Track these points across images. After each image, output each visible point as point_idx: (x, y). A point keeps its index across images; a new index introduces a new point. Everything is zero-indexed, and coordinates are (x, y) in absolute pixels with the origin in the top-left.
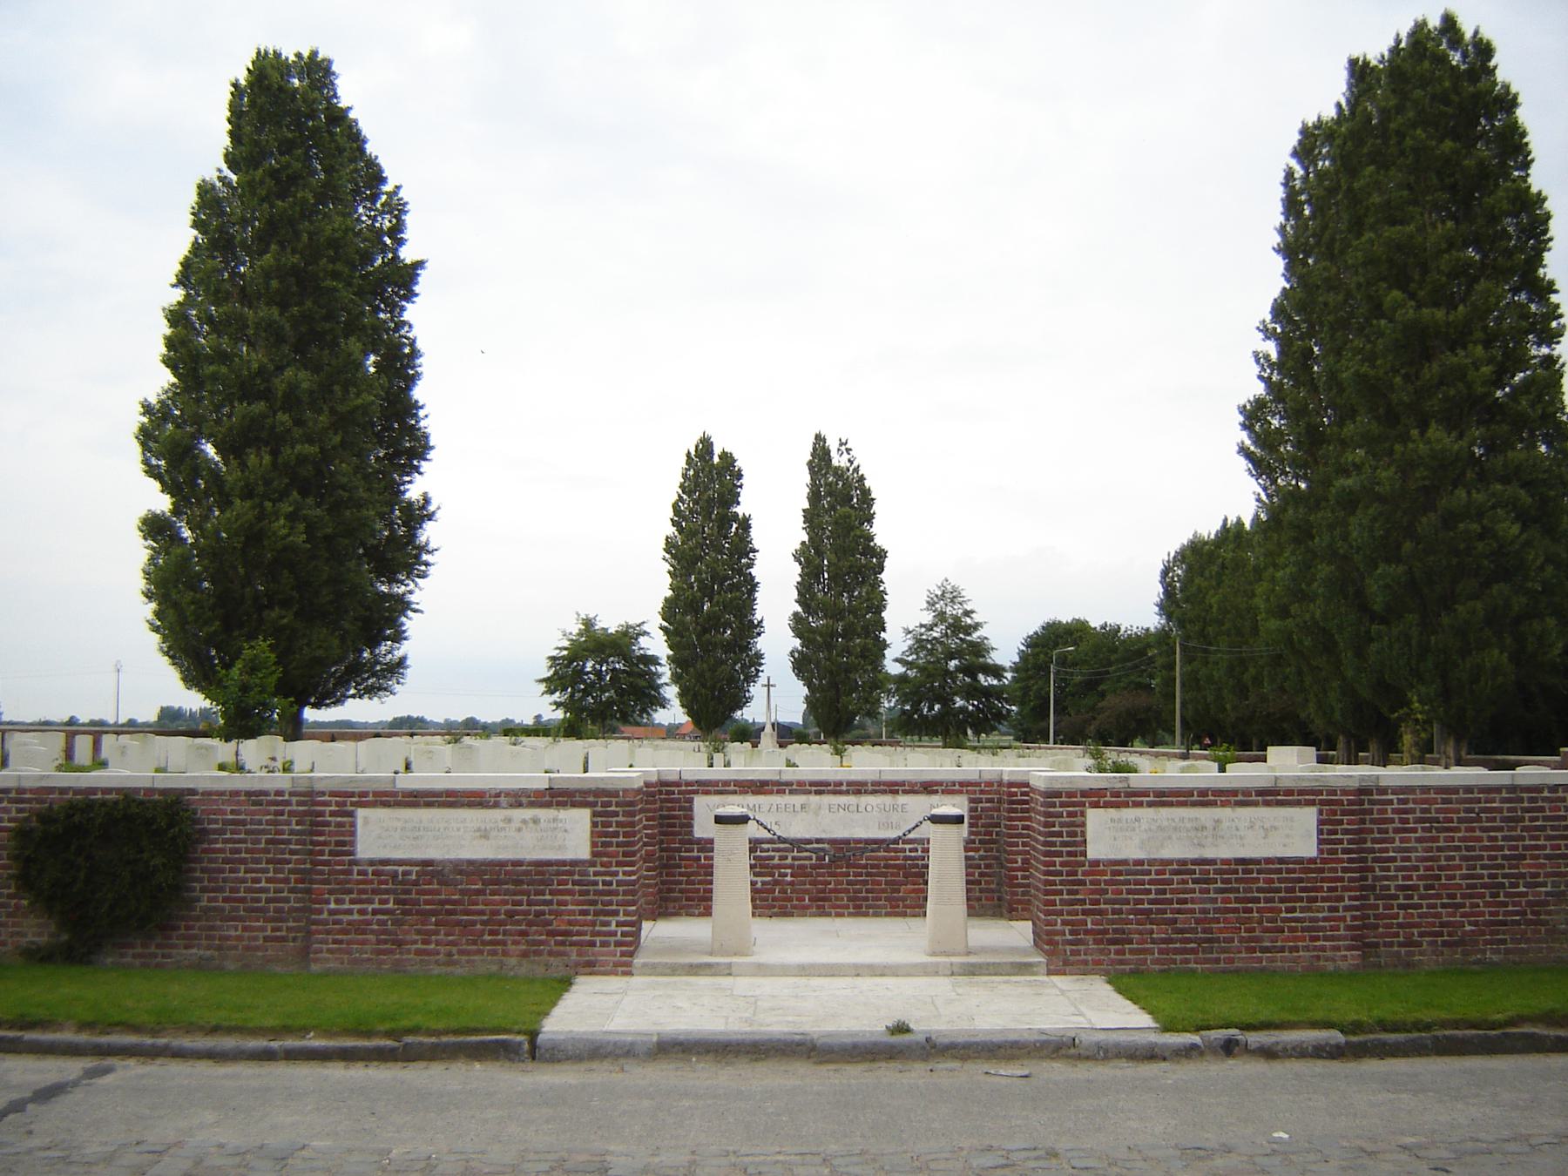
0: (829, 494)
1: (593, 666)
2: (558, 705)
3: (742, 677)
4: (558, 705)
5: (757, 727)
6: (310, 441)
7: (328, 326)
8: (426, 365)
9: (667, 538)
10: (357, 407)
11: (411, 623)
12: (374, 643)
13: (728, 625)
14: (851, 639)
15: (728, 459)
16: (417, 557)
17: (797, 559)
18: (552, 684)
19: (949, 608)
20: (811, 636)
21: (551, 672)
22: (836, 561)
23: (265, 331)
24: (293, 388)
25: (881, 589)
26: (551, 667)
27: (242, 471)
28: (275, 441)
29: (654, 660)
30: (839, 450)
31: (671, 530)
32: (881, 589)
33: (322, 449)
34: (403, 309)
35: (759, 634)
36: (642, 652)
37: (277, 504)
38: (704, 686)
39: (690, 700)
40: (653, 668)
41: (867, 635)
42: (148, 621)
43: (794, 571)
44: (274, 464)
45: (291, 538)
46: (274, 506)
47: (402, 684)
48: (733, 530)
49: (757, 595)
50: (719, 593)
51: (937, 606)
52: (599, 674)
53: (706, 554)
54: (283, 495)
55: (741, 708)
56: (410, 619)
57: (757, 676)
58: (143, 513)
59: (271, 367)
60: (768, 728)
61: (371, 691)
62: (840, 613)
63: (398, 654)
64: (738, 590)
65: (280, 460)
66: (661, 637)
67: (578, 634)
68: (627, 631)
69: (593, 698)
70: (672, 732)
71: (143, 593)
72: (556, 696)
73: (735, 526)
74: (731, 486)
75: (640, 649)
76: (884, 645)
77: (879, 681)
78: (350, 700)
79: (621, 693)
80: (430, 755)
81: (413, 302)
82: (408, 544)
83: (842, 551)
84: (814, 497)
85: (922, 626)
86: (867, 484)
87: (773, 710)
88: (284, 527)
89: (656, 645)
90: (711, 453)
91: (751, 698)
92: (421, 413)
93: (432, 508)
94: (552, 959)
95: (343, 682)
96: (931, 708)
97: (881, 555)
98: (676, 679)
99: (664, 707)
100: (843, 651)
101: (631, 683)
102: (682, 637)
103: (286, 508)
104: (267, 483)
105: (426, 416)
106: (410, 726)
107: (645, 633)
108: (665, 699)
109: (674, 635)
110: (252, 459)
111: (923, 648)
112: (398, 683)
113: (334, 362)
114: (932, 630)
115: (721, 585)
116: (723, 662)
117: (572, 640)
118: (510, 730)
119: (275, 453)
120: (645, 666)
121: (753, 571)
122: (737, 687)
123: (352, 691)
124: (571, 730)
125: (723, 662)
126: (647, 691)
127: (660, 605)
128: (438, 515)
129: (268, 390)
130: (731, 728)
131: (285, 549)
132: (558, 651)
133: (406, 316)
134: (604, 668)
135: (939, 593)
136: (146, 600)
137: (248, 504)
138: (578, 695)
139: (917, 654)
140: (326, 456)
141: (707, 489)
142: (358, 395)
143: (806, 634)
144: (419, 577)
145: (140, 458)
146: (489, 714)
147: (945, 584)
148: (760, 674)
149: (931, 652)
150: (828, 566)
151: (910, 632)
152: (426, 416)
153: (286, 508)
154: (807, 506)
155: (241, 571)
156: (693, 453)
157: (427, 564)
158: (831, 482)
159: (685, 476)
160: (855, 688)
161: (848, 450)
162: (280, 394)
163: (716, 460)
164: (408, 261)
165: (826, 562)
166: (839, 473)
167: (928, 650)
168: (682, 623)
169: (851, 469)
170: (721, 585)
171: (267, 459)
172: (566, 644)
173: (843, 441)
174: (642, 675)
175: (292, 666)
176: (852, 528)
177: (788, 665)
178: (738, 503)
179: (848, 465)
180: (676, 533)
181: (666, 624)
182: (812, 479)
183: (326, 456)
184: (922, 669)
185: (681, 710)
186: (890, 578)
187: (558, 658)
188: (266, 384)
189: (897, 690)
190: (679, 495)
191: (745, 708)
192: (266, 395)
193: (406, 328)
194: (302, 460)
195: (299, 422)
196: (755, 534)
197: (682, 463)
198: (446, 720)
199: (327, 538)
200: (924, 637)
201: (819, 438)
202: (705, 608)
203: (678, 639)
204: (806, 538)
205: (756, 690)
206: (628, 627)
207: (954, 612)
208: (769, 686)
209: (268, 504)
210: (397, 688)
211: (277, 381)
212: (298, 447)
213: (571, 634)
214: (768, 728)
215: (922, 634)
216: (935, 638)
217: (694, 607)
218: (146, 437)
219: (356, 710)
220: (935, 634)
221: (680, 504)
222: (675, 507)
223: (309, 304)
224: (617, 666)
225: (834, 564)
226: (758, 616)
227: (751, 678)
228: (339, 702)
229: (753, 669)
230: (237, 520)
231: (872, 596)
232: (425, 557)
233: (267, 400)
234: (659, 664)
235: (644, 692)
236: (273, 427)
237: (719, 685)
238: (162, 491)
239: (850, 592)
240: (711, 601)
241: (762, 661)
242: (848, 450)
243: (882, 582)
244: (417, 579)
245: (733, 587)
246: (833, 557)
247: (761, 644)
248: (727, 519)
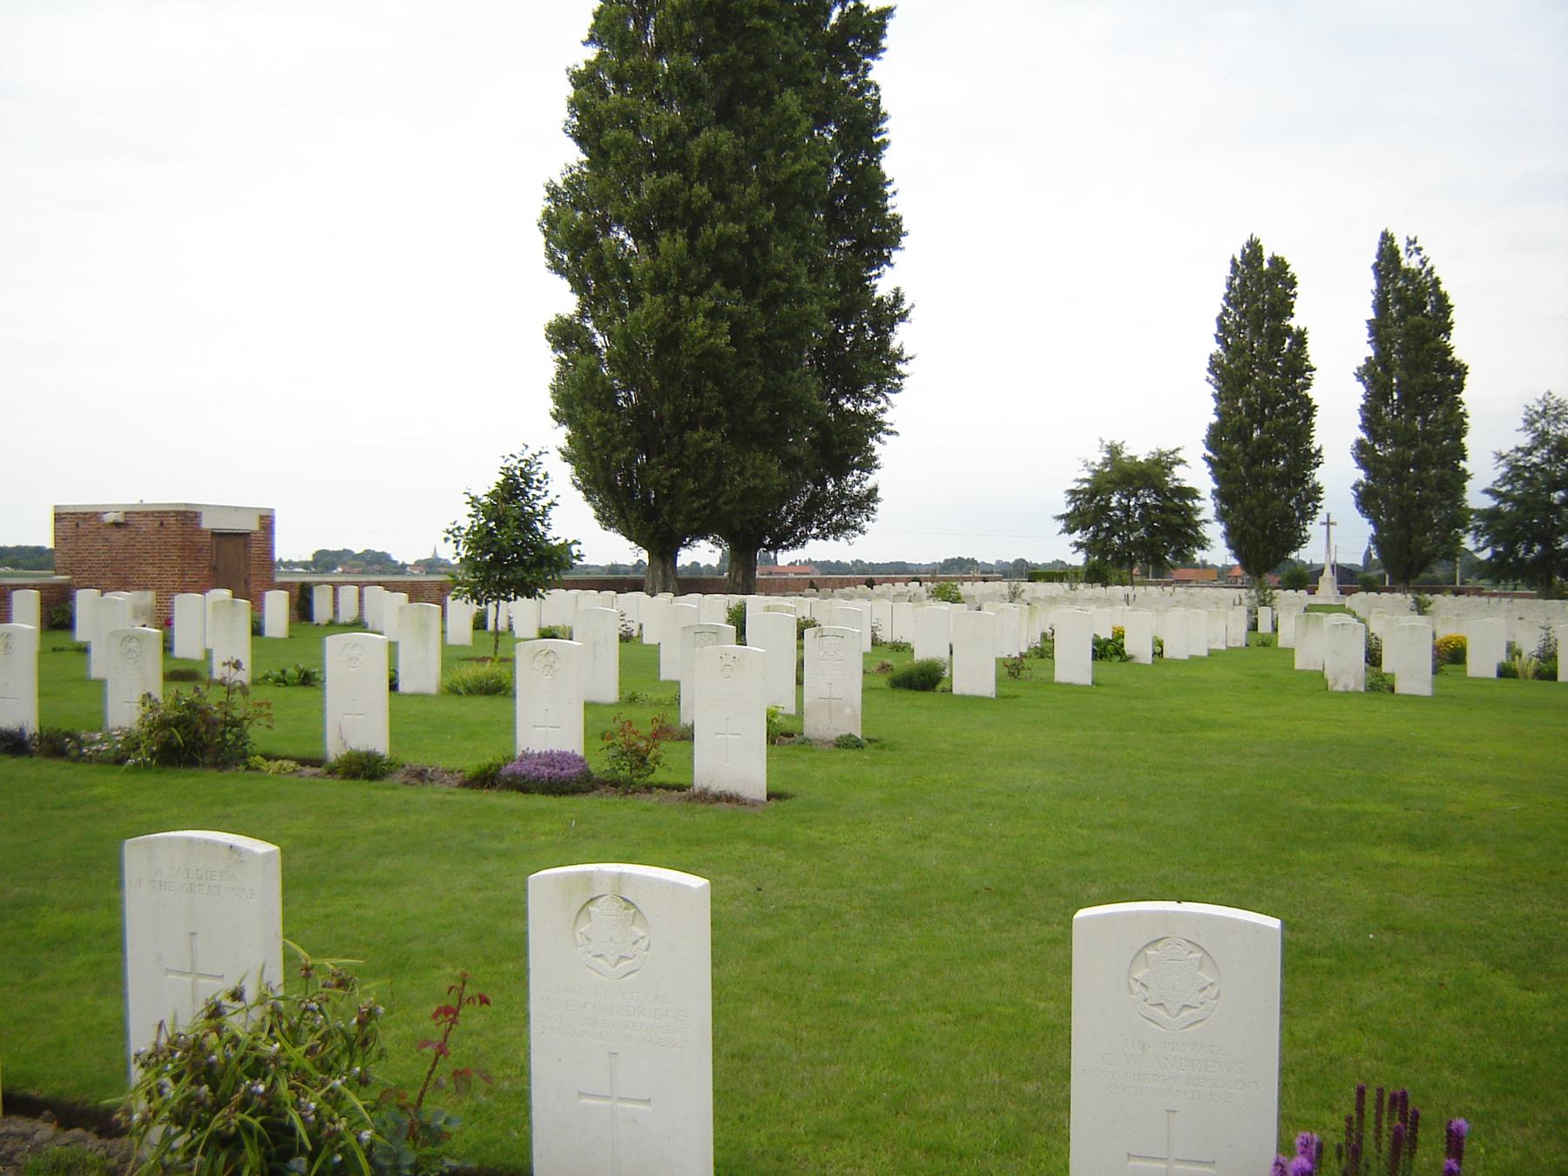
0: (1398, 301)
1: (1119, 501)
2: (1079, 546)
3: (1297, 514)
4: (1079, 546)
5: (1314, 569)
6: (737, 219)
7: (757, 77)
8: (893, 130)
9: (1211, 356)
10: (795, 175)
11: (882, 449)
12: (841, 471)
13: (1280, 454)
14: (1425, 469)
15: (1279, 265)
16: (887, 367)
17: (1360, 377)
18: (1072, 522)
19: (1552, 428)
20: (1378, 466)
21: (1071, 508)
22: (1407, 379)
23: (678, 85)
24: (711, 153)
25: (1461, 410)
26: (1070, 502)
27: (654, 259)
28: (694, 221)
29: (1191, 493)
30: (1407, 250)
31: (1215, 348)
32: (1461, 410)
33: (751, 230)
34: (867, 68)
35: (1317, 465)
36: (1176, 483)
37: (696, 300)
38: (1252, 524)
39: (1236, 539)
40: (1190, 503)
41: (1444, 464)
42: (560, 450)
43: (1356, 393)
44: (691, 249)
45: (712, 340)
46: (692, 301)
47: (873, 521)
48: (1286, 346)
49: (1314, 420)
50: (1271, 419)
51: (1538, 425)
52: (1126, 509)
53: (1255, 374)
54: (704, 286)
55: (1295, 549)
56: (884, 443)
57: (1314, 512)
58: (551, 318)
59: (685, 128)
60: (1328, 572)
61: (838, 530)
62: (1412, 439)
63: (869, 484)
64: (1291, 415)
65: (699, 244)
66: (1205, 469)
67: (1102, 464)
68: (1159, 458)
69: (1120, 537)
70: (1222, 577)
71: (551, 414)
72: (1077, 536)
73: (1288, 341)
74: (1282, 295)
75: (1174, 480)
76: (1464, 476)
77: (1458, 518)
78: (811, 541)
79: (1152, 532)
80: (551, 658)
81: (880, 58)
82: (879, 351)
83: (1415, 366)
84: (1381, 305)
85: (1518, 449)
86: (1442, 288)
87: (1333, 552)
88: (703, 325)
89: (1196, 475)
90: (1260, 259)
91: (1308, 538)
92: (889, 190)
93: (905, 307)
94: (1348, 599)
95: (805, 519)
96: (1529, 550)
97: (1461, 371)
98: (1222, 516)
99: (1203, 548)
100: (1415, 483)
101: (1163, 520)
102: (1229, 469)
103: (706, 303)
104: (683, 273)
105: (895, 193)
106: (870, 577)
107: (1181, 462)
108: (1204, 538)
109: (1220, 467)
110: (663, 243)
111: (1519, 477)
112: (868, 520)
113: (767, 121)
114: (1530, 454)
115: (1273, 409)
116: (1275, 497)
117: (1094, 471)
118: (444, 632)
119: (692, 235)
120: (1181, 500)
121: (1310, 393)
122: (1292, 526)
123: (815, 531)
124: (1095, 575)
125: (1275, 497)
126: (1183, 530)
127: (1203, 433)
128: (911, 315)
129: (683, 157)
130: (1284, 571)
131: (704, 354)
132: (1078, 484)
133: (872, 76)
134: (1132, 503)
135: (1540, 409)
136: (556, 423)
137: (659, 299)
138: (1102, 535)
139: (1512, 484)
140: (758, 239)
141: (1255, 300)
142: (795, 160)
143: (1372, 464)
144: (890, 390)
145: (542, 249)
146: (988, 554)
147: (1547, 397)
148: (1318, 510)
149: (1529, 482)
150: (1398, 385)
151: (1503, 458)
152: (895, 193)
153: (706, 303)
154: (1372, 316)
155: (655, 383)
156: (1239, 259)
157: (901, 377)
158: (1400, 288)
159: (1230, 286)
160: (1430, 526)
161: (1418, 250)
162: (696, 160)
163: (1266, 266)
164: (873, 9)
165: (1395, 381)
166: (1410, 275)
167: (1525, 479)
168: (1228, 452)
169: (1423, 272)
170: (1273, 409)
171: (681, 242)
172: (1088, 475)
173: (1412, 238)
174: (1177, 511)
175: (721, 500)
176: (1426, 340)
177: (1350, 498)
178: (1292, 315)
179: (1421, 267)
180: (1221, 351)
181: (1210, 454)
182: (1378, 284)
183: (758, 239)
184: (1518, 502)
185: (1228, 551)
186: (1471, 397)
187: (1080, 492)
188: (680, 151)
189: (1487, 528)
190: (1224, 308)
191: (1300, 550)
192: (681, 164)
193: (872, 91)
194: (725, 243)
195: (721, 196)
196: (1311, 349)
197: (1227, 271)
198: (998, 562)
199: (760, 339)
200: (1521, 463)
201: (1386, 238)
202: (1254, 435)
203: (1224, 471)
204: (1371, 353)
205: (1314, 529)
206: (1161, 454)
207: (1559, 433)
208: (1328, 523)
209: (684, 299)
210: (867, 525)
211: (691, 145)
212: (720, 226)
213: (1093, 463)
214: (1328, 572)
215: (1518, 461)
216: (1534, 464)
217: (1242, 435)
218: (551, 222)
219: (818, 550)
220: (1535, 460)
221: (1225, 318)
222: (1220, 320)
223: (732, 48)
224: (1148, 501)
225: (1405, 382)
226: (1316, 445)
227: (1308, 515)
228: (799, 542)
229: (1310, 505)
230: (646, 319)
231: (1450, 419)
232: (900, 367)
233: (682, 170)
234: (1198, 498)
235: (1179, 531)
236: (688, 202)
237: (1271, 522)
238: (572, 291)
239: (1425, 415)
240: (1261, 426)
241: (1321, 495)
242: (1418, 250)
243: (1461, 402)
244: (887, 394)
245: (1288, 412)
246: (1403, 374)
247: (1320, 475)
248: (1278, 333)
